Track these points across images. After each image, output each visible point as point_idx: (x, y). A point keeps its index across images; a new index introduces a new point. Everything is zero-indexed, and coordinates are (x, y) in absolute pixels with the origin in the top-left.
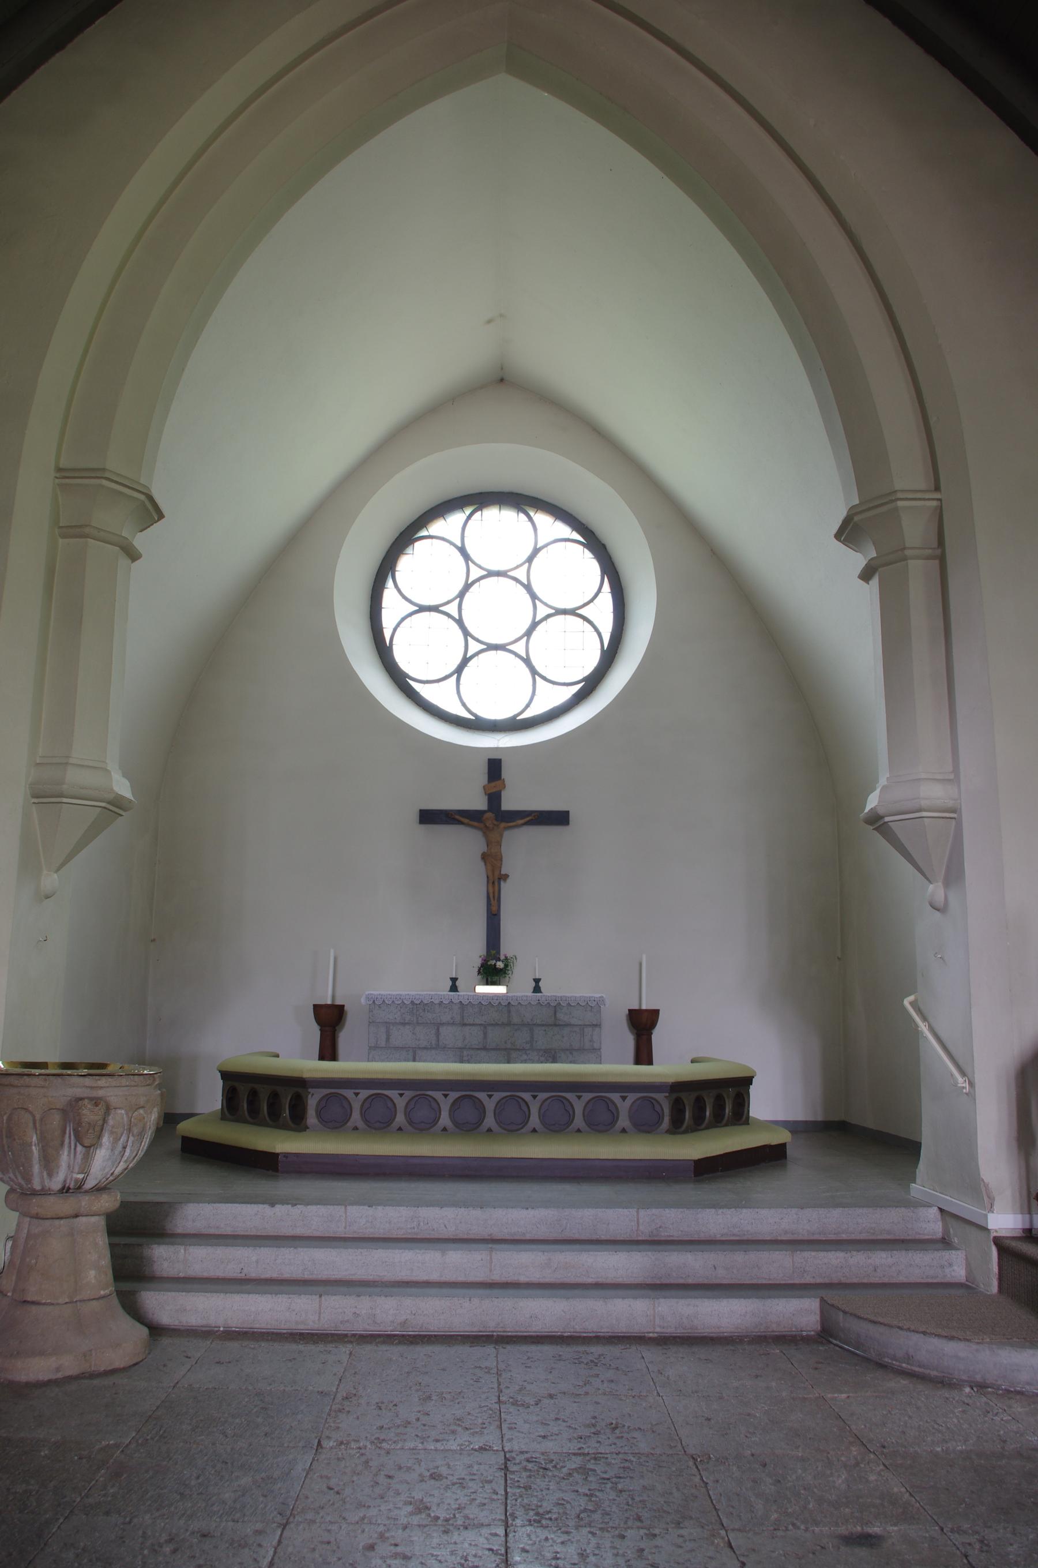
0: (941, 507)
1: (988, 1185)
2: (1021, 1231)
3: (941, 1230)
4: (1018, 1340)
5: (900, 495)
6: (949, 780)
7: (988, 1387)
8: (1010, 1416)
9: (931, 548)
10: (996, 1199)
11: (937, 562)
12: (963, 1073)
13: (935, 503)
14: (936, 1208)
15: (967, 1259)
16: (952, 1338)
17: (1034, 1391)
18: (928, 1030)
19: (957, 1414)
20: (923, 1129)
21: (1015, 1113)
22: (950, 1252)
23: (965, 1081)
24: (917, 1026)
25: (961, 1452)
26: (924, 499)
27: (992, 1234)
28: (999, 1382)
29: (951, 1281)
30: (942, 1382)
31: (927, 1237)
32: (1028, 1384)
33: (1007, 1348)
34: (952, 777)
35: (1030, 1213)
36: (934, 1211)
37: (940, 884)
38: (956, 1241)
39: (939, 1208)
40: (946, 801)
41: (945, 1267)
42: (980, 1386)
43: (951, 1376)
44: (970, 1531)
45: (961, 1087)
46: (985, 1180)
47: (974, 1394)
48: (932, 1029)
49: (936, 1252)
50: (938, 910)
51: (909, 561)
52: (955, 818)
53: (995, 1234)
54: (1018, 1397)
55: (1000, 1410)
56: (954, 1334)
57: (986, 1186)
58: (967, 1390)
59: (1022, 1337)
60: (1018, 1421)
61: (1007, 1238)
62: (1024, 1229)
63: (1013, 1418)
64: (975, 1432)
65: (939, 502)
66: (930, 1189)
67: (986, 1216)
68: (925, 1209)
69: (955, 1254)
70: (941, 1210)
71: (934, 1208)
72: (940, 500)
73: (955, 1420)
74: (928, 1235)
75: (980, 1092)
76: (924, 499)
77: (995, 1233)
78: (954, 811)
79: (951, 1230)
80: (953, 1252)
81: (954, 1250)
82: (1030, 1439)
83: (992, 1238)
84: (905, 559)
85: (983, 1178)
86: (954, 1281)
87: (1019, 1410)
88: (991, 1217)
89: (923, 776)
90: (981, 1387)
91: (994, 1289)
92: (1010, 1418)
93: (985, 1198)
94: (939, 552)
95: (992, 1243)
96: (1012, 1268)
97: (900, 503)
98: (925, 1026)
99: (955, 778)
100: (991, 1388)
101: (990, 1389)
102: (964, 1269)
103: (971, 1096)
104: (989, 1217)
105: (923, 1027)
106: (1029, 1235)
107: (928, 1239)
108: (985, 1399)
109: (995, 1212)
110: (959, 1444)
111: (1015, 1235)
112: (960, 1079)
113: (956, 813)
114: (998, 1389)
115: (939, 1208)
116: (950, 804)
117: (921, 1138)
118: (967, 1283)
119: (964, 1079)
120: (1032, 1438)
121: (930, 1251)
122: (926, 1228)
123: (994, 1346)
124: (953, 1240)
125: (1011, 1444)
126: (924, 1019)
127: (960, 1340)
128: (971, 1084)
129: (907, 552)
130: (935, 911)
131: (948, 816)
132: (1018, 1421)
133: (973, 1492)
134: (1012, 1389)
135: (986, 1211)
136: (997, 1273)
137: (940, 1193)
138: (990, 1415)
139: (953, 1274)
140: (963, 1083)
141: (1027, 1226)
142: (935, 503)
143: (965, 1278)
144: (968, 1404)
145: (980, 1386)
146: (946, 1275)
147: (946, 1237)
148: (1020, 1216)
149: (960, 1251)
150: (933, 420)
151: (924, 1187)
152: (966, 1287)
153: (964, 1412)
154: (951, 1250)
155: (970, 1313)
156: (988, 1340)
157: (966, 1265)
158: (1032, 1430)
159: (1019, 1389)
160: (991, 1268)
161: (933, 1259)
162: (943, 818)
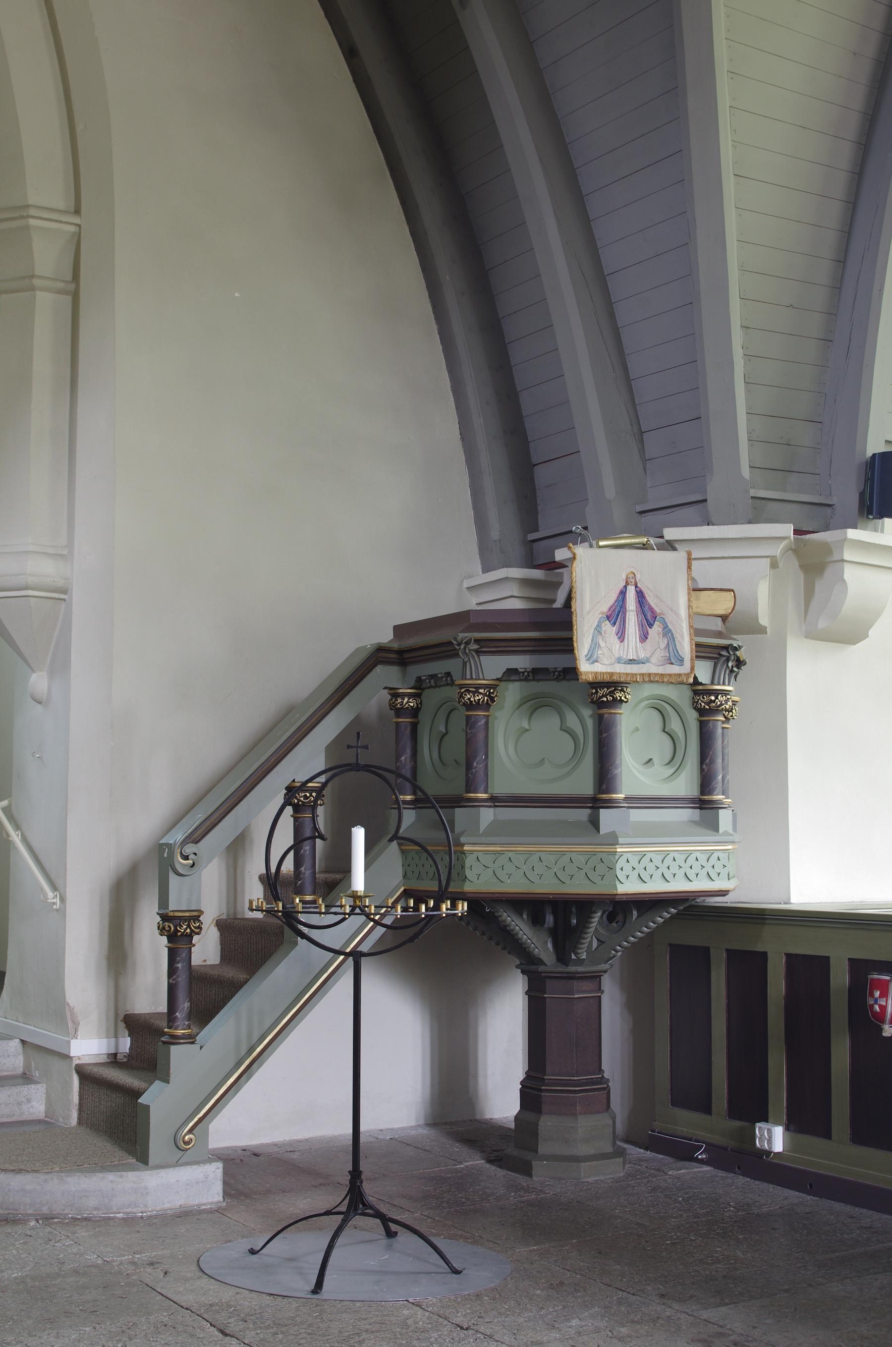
0: (80, 233)
1: (73, 1009)
2: (105, 1057)
3: (22, 1064)
4: (89, 1166)
5: (32, 212)
6: (62, 556)
7: (54, 1218)
8: (73, 1241)
9: (63, 281)
10: (81, 1023)
11: (69, 299)
12: (54, 888)
13: (72, 229)
14: (18, 1041)
15: (47, 1093)
16: (20, 1171)
17: (102, 1215)
18: (21, 841)
19: (18, 1246)
20: (8, 953)
21: (106, 930)
22: (29, 1086)
23: (56, 896)
24: (8, 835)
25: (16, 1278)
26: (61, 222)
27: (74, 1061)
28: (66, 1212)
29: (28, 1119)
30: (6, 1220)
31: (5, 1074)
32: (96, 1209)
33: (76, 1174)
34: (65, 552)
35: (116, 1036)
36: (16, 1043)
37: (44, 673)
38: (37, 1075)
39: (20, 1039)
40: (55, 580)
41: (23, 1104)
42: (46, 1218)
43: (16, 1212)
44: (14, 1342)
45: (52, 902)
46: (70, 1004)
47: (39, 1226)
48: (25, 840)
49: (13, 1088)
50: (40, 703)
51: (38, 293)
52: (64, 600)
53: (78, 1062)
54: (84, 1223)
55: (64, 1237)
56: (23, 1167)
57: (72, 1010)
58: (33, 1223)
59: (94, 1163)
60: (80, 1244)
61: (90, 1064)
62: (109, 1054)
63: (76, 1243)
64: (34, 1259)
65: (78, 228)
66: (12, 1020)
67: (69, 1043)
68: (6, 1042)
69: (34, 1089)
70: (23, 1042)
71: (15, 1040)
72: (79, 226)
73: (14, 1252)
74: (8, 1072)
75: (72, 908)
76: (61, 222)
77: (77, 1061)
78: (65, 592)
79: (33, 1064)
80: (33, 1086)
81: (34, 1084)
82: (89, 1257)
83: (74, 1066)
84: (33, 289)
85: (69, 1002)
86: (31, 1119)
87: (83, 1234)
88: (74, 1043)
89: (32, 548)
90: (47, 1219)
91: (74, 1120)
92: (73, 1242)
93: (70, 1024)
94: (72, 287)
95: (74, 1072)
96: (92, 1095)
97: (32, 222)
98: (18, 835)
99: (65, 556)
100: (56, 1218)
101: (56, 1220)
102: (44, 1104)
103: (62, 912)
104: (72, 1044)
105: (15, 838)
106: (113, 1060)
107: (7, 1076)
108: (50, 1229)
109: (78, 1037)
110: (15, 1272)
111: (99, 1062)
112: (50, 894)
113: (66, 594)
114: (65, 1218)
115: (20, 1039)
116: (60, 583)
117: (6, 968)
118: (46, 1119)
119: (55, 894)
120: (90, 1256)
121: (6, 1088)
122: (5, 1064)
123: (63, 1174)
124: (34, 1075)
125: (69, 1265)
126: (17, 827)
127: (28, 1171)
128: (63, 900)
129: (36, 282)
130: (36, 703)
131: (57, 597)
132: (80, 1244)
133: (21, 1310)
134: (79, 1217)
135: (69, 1037)
136: (78, 1104)
137: (24, 1023)
138: (52, 1243)
139: (31, 1110)
140: (53, 898)
141: (113, 1051)
142: (72, 229)
143: (44, 1114)
144: (30, 1236)
145: (46, 1218)
146: (24, 1113)
147: (27, 1073)
148: (105, 1041)
149: (40, 1085)
150: (79, 128)
151: (6, 1018)
152: (45, 1124)
153: (25, 1243)
154: (31, 1084)
155: (44, 1146)
156: (58, 1169)
157: (46, 1100)
158: (93, 1250)
159: (86, 1215)
160: (71, 1099)
161: (9, 1096)
162: (51, 598)
